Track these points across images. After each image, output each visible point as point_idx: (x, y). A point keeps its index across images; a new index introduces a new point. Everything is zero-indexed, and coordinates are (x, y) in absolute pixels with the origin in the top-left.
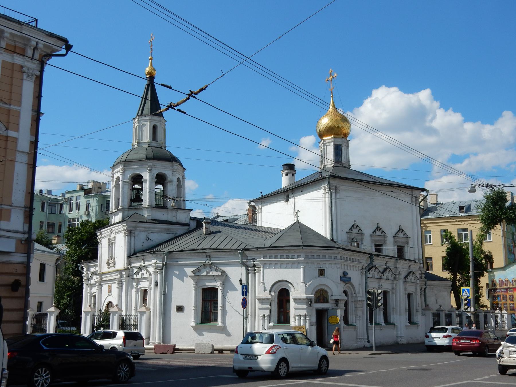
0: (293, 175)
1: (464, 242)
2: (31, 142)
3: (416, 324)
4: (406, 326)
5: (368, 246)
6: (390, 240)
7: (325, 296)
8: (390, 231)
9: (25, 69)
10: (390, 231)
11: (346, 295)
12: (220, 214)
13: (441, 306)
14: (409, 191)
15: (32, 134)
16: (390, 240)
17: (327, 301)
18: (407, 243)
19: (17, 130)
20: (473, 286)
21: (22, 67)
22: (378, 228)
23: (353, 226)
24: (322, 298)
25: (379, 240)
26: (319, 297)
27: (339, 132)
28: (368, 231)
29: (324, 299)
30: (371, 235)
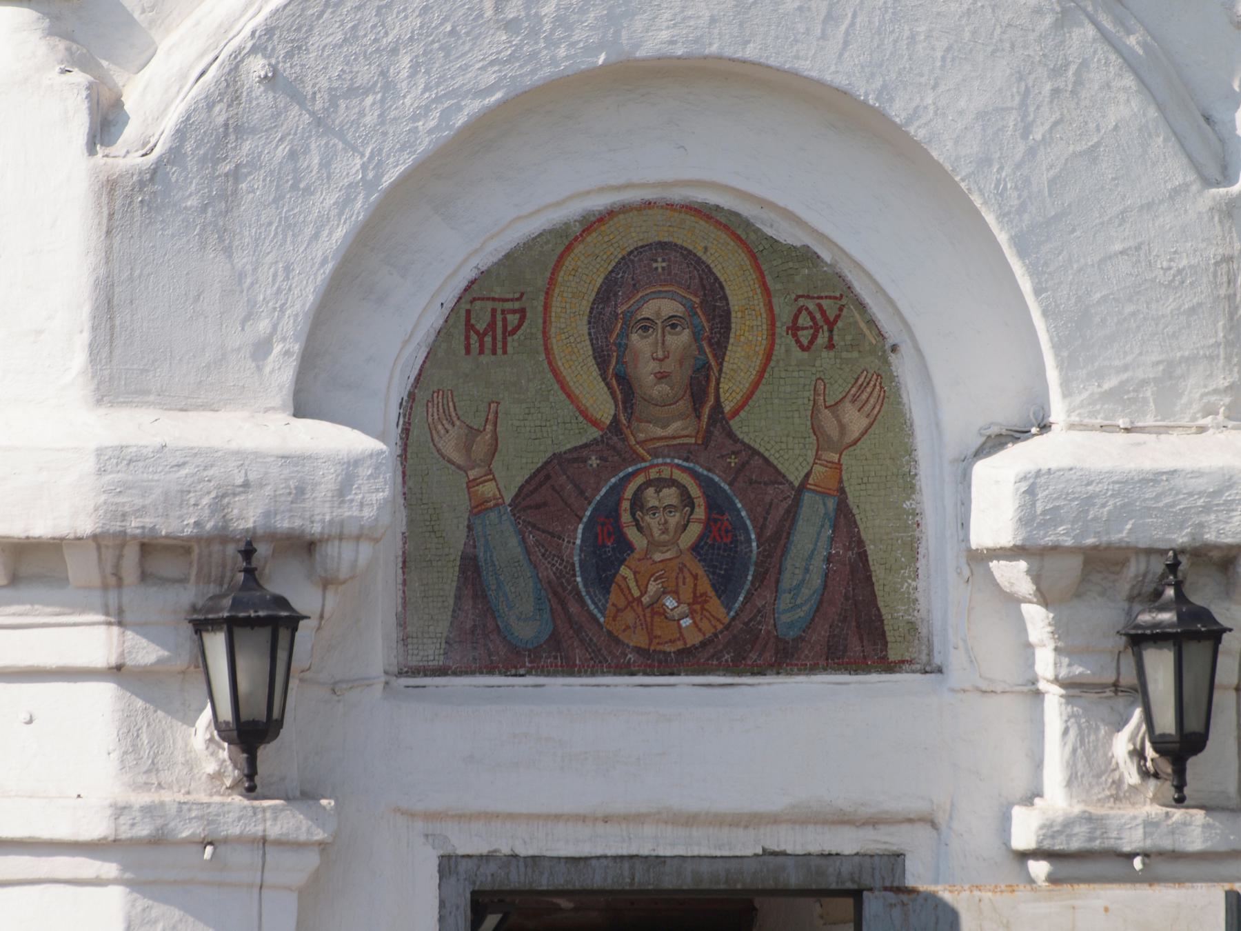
7: (775, 432)
17: (858, 628)
24: (665, 531)
26: (543, 496)
29: (730, 555)
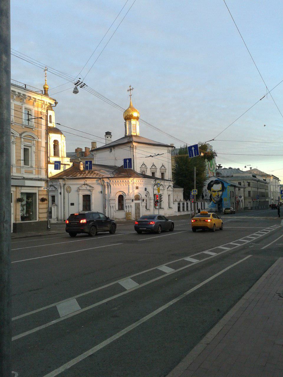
0: (111, 137)
1: (194, 156)
2: (46, 143)
3: (171, 208)
4: (168, 209)
5: (158, 175)
6: (158, 170)
8: (158, 166)
9: (42, 113)
10: (158, 166)
11: (146, 197)
12: (266, 180)
13: (180, 200)
14: (166, 148)
15: (46, 140)
16: (158, 170)
17: (139, 200)
18: (166, 171)
19: (41, 138)
20: (218, 256)
21: (41, 112)
22: (153, 165)
23: (143, 164)
25: (163, 171)
27: (137, 118)
28: (149, 167)
29: (138, 199)
30: (150, 168)
